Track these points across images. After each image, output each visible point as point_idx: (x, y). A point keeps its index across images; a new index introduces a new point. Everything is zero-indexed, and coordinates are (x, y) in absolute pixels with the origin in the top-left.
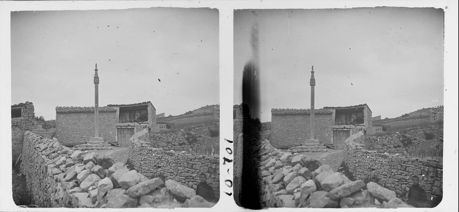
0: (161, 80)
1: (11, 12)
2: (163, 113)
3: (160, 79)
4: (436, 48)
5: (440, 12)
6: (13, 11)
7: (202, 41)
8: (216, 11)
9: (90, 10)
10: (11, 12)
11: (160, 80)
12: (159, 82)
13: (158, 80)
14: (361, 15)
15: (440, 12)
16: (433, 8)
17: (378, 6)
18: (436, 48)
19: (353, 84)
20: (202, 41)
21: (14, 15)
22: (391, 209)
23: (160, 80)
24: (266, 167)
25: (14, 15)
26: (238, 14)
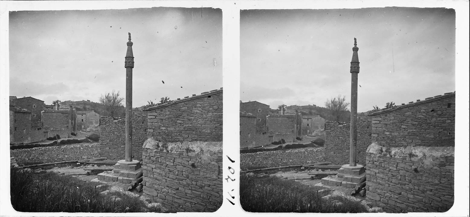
0: (164, 82)
1: (9, 11)
2: (208, 96)
3: (164, 81)
4: (446, 49)
5: (451, 12)
6: (11, 11)
7: (206, 42)
8: (219, 11)
9: (84, 10)
10: (9, 11)
11: (163, 82)
12: (163, 84)
13: (162, 82)
14: (370, 15)
15: (451, 12)
16: (211, 8)
17: (39, 99)
18: (446, 49)
19: (361, 86)
20: (206, 42)
21: (13, 15)
22: (384, 7)
23: (163, 82)
24: (269, 179)
25: (13, 15)
26: (244, 14)
